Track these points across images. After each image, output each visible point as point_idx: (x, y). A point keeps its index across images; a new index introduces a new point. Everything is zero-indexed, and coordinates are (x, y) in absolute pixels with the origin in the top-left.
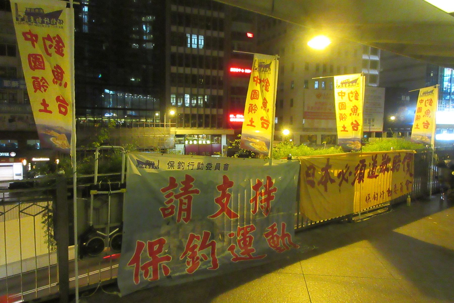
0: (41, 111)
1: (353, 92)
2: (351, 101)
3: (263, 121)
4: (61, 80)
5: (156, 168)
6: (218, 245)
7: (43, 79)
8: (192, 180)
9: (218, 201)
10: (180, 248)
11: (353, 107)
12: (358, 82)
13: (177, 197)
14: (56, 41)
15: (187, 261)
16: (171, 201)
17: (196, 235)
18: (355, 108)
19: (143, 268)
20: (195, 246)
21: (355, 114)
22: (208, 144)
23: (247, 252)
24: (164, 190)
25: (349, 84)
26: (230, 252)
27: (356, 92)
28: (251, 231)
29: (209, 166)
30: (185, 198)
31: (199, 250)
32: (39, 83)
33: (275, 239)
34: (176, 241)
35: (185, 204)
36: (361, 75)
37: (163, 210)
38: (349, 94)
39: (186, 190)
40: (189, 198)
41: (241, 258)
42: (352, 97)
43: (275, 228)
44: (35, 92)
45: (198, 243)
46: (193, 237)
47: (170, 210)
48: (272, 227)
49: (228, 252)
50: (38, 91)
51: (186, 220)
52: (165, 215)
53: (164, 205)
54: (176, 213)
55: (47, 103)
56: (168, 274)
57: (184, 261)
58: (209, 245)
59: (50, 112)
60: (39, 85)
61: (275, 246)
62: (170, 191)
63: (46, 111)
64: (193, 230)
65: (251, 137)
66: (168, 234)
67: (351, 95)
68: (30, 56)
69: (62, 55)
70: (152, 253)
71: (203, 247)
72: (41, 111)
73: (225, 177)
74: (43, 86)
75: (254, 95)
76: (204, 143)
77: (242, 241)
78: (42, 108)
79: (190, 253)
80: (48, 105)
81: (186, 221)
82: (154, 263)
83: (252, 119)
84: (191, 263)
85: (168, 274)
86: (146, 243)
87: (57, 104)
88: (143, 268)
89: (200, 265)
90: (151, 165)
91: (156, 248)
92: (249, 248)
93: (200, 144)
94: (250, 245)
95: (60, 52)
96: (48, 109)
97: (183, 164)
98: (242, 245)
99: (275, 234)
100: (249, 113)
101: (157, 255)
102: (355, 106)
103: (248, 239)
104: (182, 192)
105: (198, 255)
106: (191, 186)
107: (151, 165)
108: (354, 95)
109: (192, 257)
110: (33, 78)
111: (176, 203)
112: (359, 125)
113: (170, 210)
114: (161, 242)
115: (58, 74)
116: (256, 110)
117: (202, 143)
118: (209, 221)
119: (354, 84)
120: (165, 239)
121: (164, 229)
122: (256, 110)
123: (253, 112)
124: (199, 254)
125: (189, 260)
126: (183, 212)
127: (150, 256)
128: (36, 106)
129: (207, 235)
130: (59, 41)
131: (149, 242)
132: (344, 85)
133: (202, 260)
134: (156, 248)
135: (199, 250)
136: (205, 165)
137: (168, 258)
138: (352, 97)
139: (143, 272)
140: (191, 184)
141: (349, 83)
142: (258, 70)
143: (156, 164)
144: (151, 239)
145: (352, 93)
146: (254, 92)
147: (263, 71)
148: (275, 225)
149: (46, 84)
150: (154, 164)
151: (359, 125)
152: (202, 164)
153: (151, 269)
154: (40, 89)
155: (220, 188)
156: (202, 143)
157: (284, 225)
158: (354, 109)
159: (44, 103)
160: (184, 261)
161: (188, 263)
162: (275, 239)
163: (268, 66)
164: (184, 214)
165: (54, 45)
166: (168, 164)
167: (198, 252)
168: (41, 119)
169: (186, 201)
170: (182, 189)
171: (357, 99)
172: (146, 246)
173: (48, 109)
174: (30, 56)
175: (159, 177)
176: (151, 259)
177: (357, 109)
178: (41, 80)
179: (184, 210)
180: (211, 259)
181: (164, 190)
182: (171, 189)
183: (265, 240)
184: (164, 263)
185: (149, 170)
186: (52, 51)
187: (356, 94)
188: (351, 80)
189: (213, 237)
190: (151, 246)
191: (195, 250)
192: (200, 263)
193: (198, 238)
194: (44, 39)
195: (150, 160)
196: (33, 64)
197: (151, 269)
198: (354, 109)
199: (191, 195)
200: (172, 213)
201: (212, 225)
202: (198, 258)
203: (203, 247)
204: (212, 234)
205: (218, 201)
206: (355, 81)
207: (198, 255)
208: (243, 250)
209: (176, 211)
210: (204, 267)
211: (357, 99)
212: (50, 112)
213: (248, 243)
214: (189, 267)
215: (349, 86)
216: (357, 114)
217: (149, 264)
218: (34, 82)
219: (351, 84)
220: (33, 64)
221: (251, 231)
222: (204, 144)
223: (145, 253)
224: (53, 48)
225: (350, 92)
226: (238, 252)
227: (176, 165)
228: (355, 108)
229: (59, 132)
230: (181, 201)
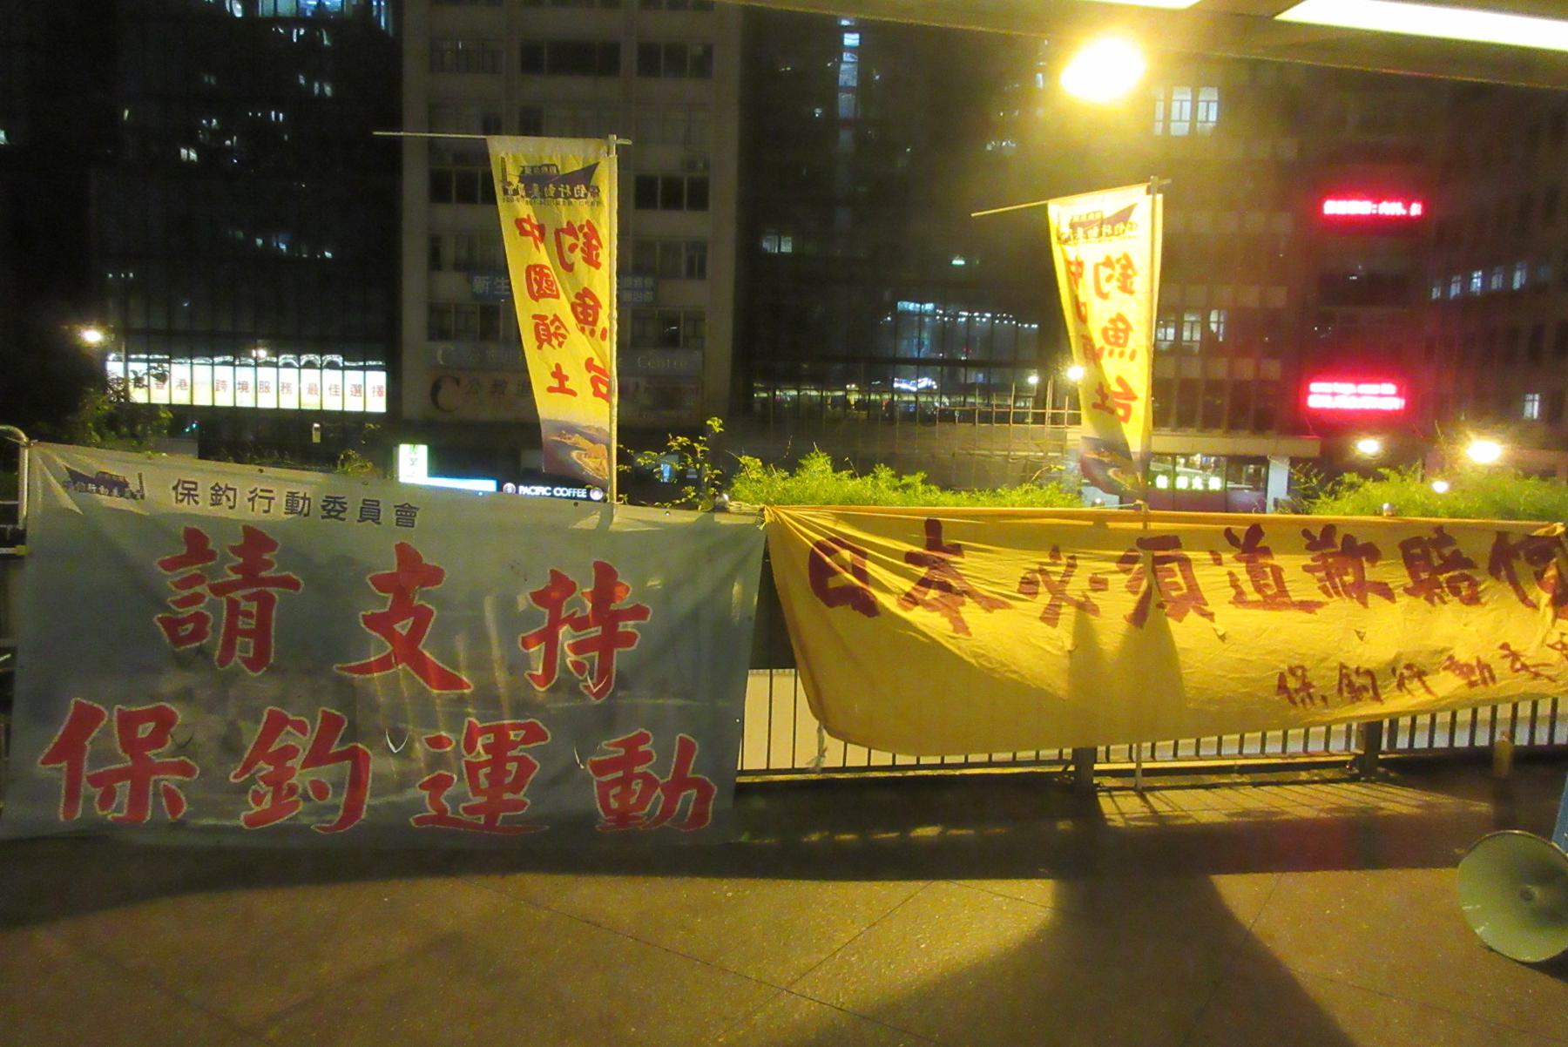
0: (551, 390)
1: (1114, 259)
2: (1103, 296)
3: (593, 373)
4: (594, 323)
5: (133, 496)
6: (381, 765)
7: (556, 318)
8: (270, 545)
9: (380, 623)
10: (230, 745)
11: (1113, 321)
12: (1132, 219)
13: (218, 590)
14: (585, 235)
15: (256, 792)
16: (198, 598)
17: (291, 717)
18: (1121, 325)
19: (96, 781)
20: (290, 752)
21: (1117, 350)
22: (1214, 492)
23: (491, 811)
24: (171, 565)
25: (1101, 226)
26: (426, 793)
27: (1126, 257)
28: (525, 741)
29: (333, 508)
30: (248, 598)
31: (304, 766)
32: (548, 329)
33: (637, 786)
34: (215, 724)
35: (248, 615)
36: (1149, 191)
37: (172, 624)
38: (1096, 267)
39: (250, 575)
40: (266, 602)
41: (459, 823)
42: (1109, 278)
43: (642, 748)
44: (540, 347)
45: (303, 743)
46: (276, 724)
47: (190, 626)
48: (631, 745)
49: (416, 793)
50: (545, 345)
51: (254, 664)
52: (177, 640)
53: (167, 608)
54: (214, 639)
55: (565, 372)
56: (179, 816)
57: (242, 789)
58: (340, 757)
59: (573, 393)
60: (548, 332)
61: (623, 817)
62: (194, 570)
63: (562, 389)
64: (281, 700)
65: (572, 429)
66: (186, 696)
67: (1104, 272)
68: (529, 269)
69: (597, 265)
70: (132, 745)
71: (317, 757)
72: (551, 390)
73: (402, 550)
74: (556, 335)
75: (539, 284)
76: (1198, 485)
77: (487, 770)
78: (555, 383)
79: (266, 768)
80: (566, 378)
81: (255, 668)
82: (139, 776)
83: (558, 366)
84: (269, 797)
85: (179, 816)
86: (111, 714)
87: (587, 377)
88: (96, 781)
89: (300, 813)
90: (120, 486)
91: (145, 730)
92: (508, 796)
93: (1181, 491)
94: (516, 786)
95: (592, 261)
96: (568, 385)
97: (231, 494)
98: (484, 783)
99: (638, 769)
100: (540, 347)
101: (150, 754)
102: (1121, 318)
103: (512, 767)
104: (234, 577)
105: (294, 781)
106: (268, 565)
107: (120, 486)
108: (1118, 270)
109: (275, 782)
110: (535, 317)
111: (214, 609)
112: (1134, 398)
113: (190, 626)
114: (164, 721)
115: (585, 307)
116: (564, 337)
117: (1190, 485)
118: (340, 680)
119: (1120, 226)
120: (180, 713)
121: (171, 682)
122: (564, 337)
123: (555, 342)
124: (302, 778)
125: (262, 787)
126: (239, 640)
127: (125, 751)
128: (540, 379)
129: (331, 723)
130: (591, 233)
131: (271, 713)
132: (1080, 230)
133: (306, 798)
134: (145, 730)
135: (304, 766)
136: (317, 504)
137: (186, 770)
138: (1109, 278)
139: (98, 792)
140: (266, 556)
141: (1101, 223)
142: (522, 192)
143: (134, 486)
144: (128, 701)
145: (1108, 263)
146: (535, 273)
147: (557, 195)
148: (643, 739)
149: (562, 331)
150: (126, 485)
151: (1134, 398)
152: (304, 498)
153: (123, 788)
154: (550, 343)
155: (383, 583)
156: (1190, 485)
157: (686, 748)
158: (1117, 330)
159: (558, 374)
160: (242, 789)
161: (258, 798)
162: (637, 786)
163: (586, 175)
164: (245, 647)
165: (580, 244)
166: (175, 488)
167: (298, 771)
168: (549, 407)
169: (253, 607)
170: (235, 570)
171: (1125, 288)
172: (110, 718)
173: (568, 385)
174: (529, 269)
175: (152, 527)
176: (127, 762)
177: (1128, 328)
178: (552, 322)
179: (246, 633)
180: (342, 800)
181: (171, 565)
182: (192, 564)
183: (589, 781)
184: (171, 780)
185: (106, 500)
186: (577, 257)
187: (1125, 267)
188: (1108, 214)
189: (354, 733)
190: (128, 723)
191: (289, 763)
192: (302, 806)
193: (301, 728)
194: (558, 232)
195: (114, 471)
196: (535, 287)
197: (123, 788)
198: (1117, 330)
199: (274, 591)
200: (197, 635)
201: (349, 695)
202: (292, 790)
203: (317, 757)
204: (352, 724)
205: (380, 623)
206: (1123, 217)
207: (294, 781)
208: (481, 799)
209: (215, 630)
210: (305, 820)
211: (1125, 288)
212: (573, 393)
213: (509, 780)
214: (257, 809)
215: (1100, 234)
216: (1128, 351)
217: (121, 775)
218: (537, 326)
219: (1107, 229)
220: (535, 287)
221: (525, 741)
222: (1196, 492)
223: (106, 735)
224: (578, 251)
225: (1102, 260)
226: (455, 800)
227: (204, 493)
228: (1121, 325)
229: (593, 440)
230: (233, 604)
